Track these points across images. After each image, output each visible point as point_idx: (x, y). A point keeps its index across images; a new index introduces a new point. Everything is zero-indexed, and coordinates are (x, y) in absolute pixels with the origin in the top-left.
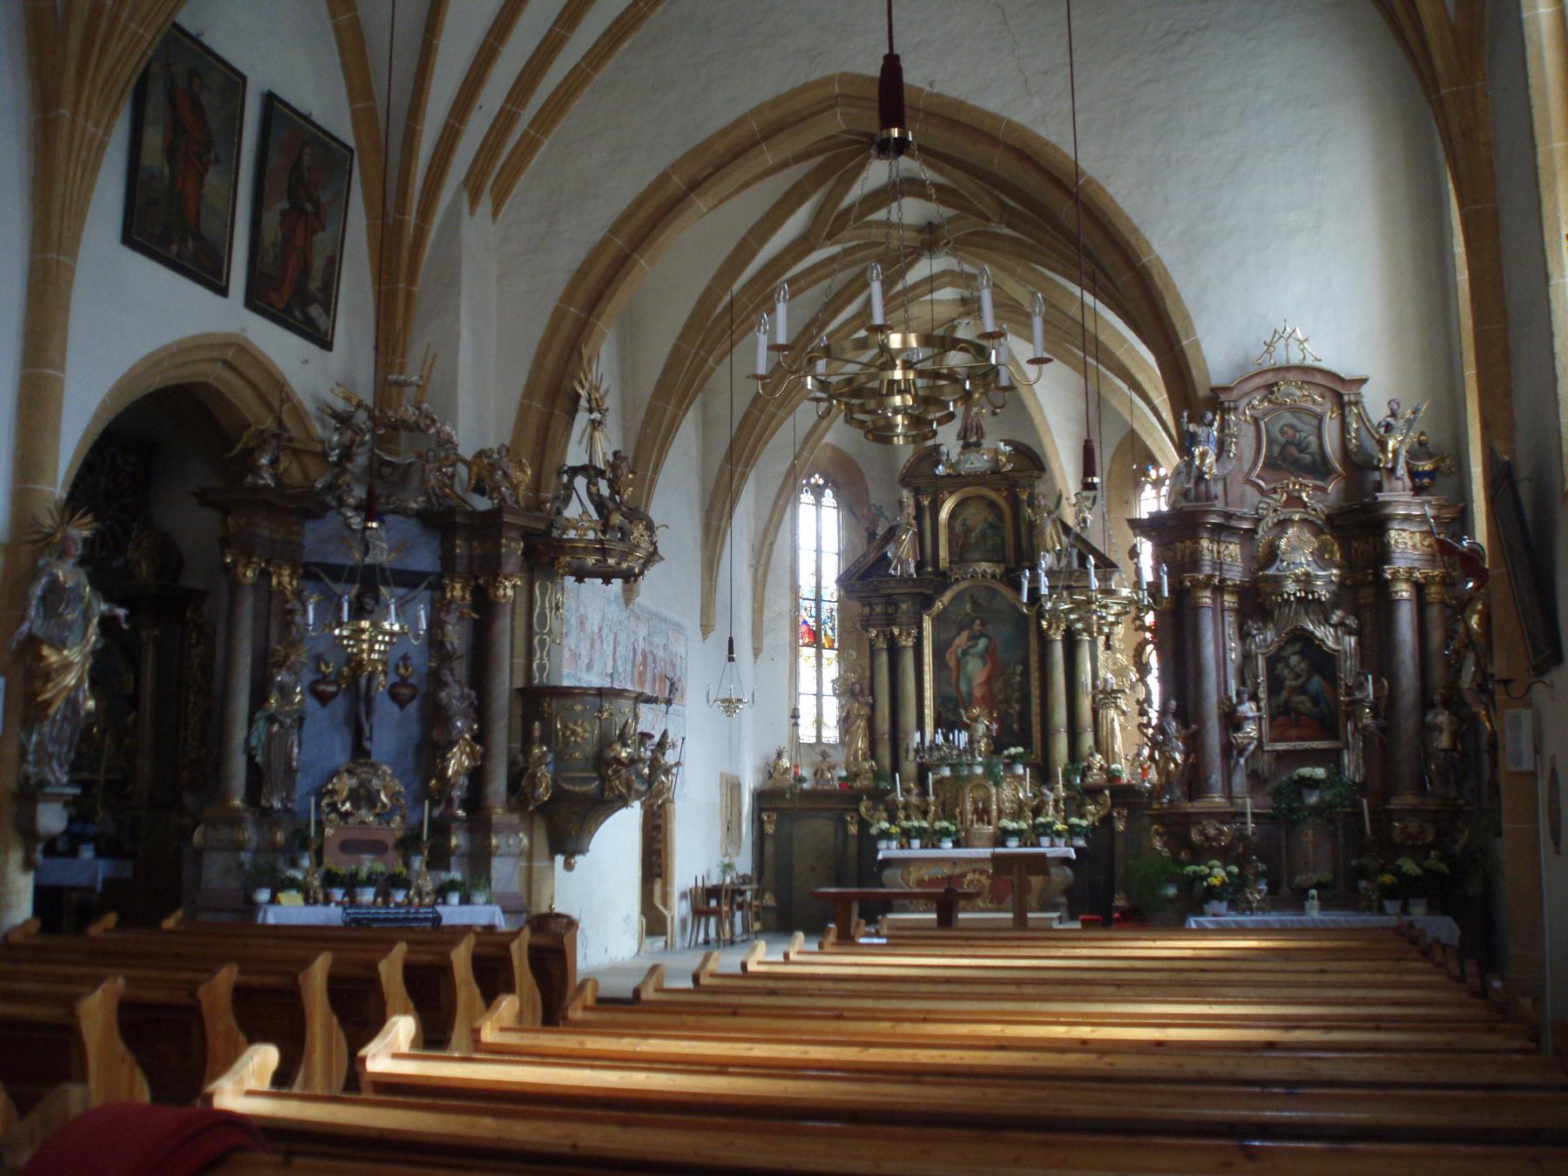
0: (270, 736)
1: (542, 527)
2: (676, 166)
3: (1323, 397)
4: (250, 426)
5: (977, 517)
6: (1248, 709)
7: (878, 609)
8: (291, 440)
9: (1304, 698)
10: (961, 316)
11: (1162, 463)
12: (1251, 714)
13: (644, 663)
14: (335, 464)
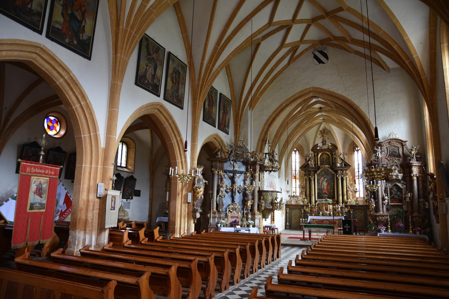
0: (220, 199)
1: (263, 164)
2: (284, 102)
3: (399, 144)
4: (217, 148)
5: (325, 157)
6: (386, 197)
7: (307, 173)
8: (223, 150)
9: (396, 196)
10: (323, 122)
11: (358, 146)
12: (387, 198)
13: (271, 184)
14: (229, 154)
